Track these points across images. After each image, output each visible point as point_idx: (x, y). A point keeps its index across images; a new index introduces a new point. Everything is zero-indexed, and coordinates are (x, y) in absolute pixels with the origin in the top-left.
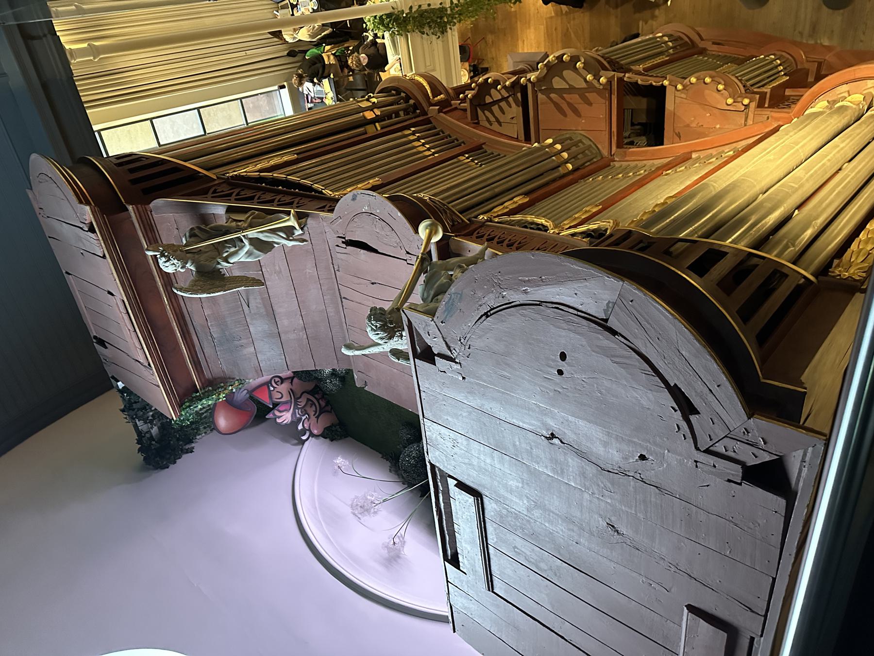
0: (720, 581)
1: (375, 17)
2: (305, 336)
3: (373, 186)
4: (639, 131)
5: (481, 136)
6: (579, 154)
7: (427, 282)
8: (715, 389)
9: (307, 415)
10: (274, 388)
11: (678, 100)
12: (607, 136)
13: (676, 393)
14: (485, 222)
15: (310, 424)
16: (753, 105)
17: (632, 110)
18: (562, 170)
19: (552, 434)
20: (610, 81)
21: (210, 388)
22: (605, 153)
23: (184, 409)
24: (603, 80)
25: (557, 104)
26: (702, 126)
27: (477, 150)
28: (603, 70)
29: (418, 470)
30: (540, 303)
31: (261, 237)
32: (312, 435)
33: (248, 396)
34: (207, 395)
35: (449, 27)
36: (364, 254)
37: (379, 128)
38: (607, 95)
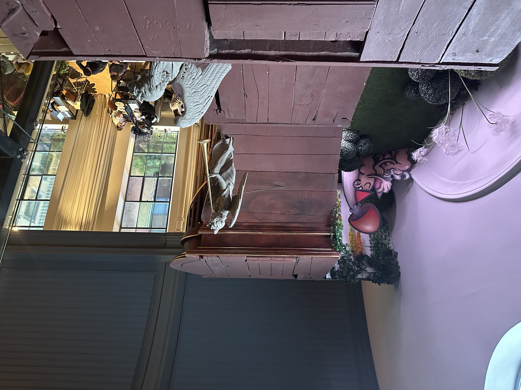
9: (391, 170)
15: (399, 170)
29: (439, 88)
32: (409, 171)
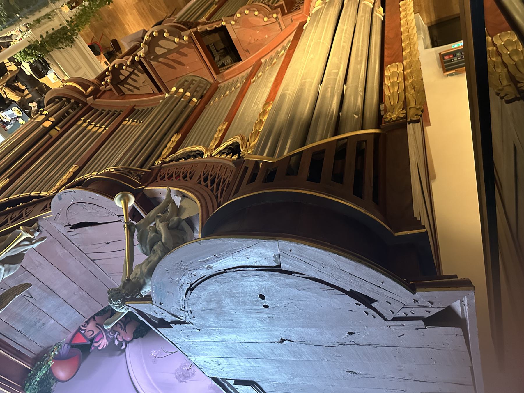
0: (436, 377)
1: (20, 52)
3: (74, 173)
4: (224, 54)
5: (130, 102)
6: (197, 88)
7: (141, 240)
9: (117, 333)
10: (85, 330)
11: (236, 31)
12: (207, 70)
13: (352, 294)
14: (161, 165)
15: (122, 337)
16: (280, 16)
17: (213, 43)
18: (191, 105)
19: (282, 339)
20: (190, 37)
21: (38, 363)
22: (211, 80)
24: (185, 38)
25: (166, 63)
26: (258, 40)
28: (182, 31)
30: (225, 271)
31: (10, 254)
32: (127, 342)
33: (69, 347)
34: (39, 369)
35: (74, 37)
36: (90, 229)
37: (59, 129)
38: (193, 46)
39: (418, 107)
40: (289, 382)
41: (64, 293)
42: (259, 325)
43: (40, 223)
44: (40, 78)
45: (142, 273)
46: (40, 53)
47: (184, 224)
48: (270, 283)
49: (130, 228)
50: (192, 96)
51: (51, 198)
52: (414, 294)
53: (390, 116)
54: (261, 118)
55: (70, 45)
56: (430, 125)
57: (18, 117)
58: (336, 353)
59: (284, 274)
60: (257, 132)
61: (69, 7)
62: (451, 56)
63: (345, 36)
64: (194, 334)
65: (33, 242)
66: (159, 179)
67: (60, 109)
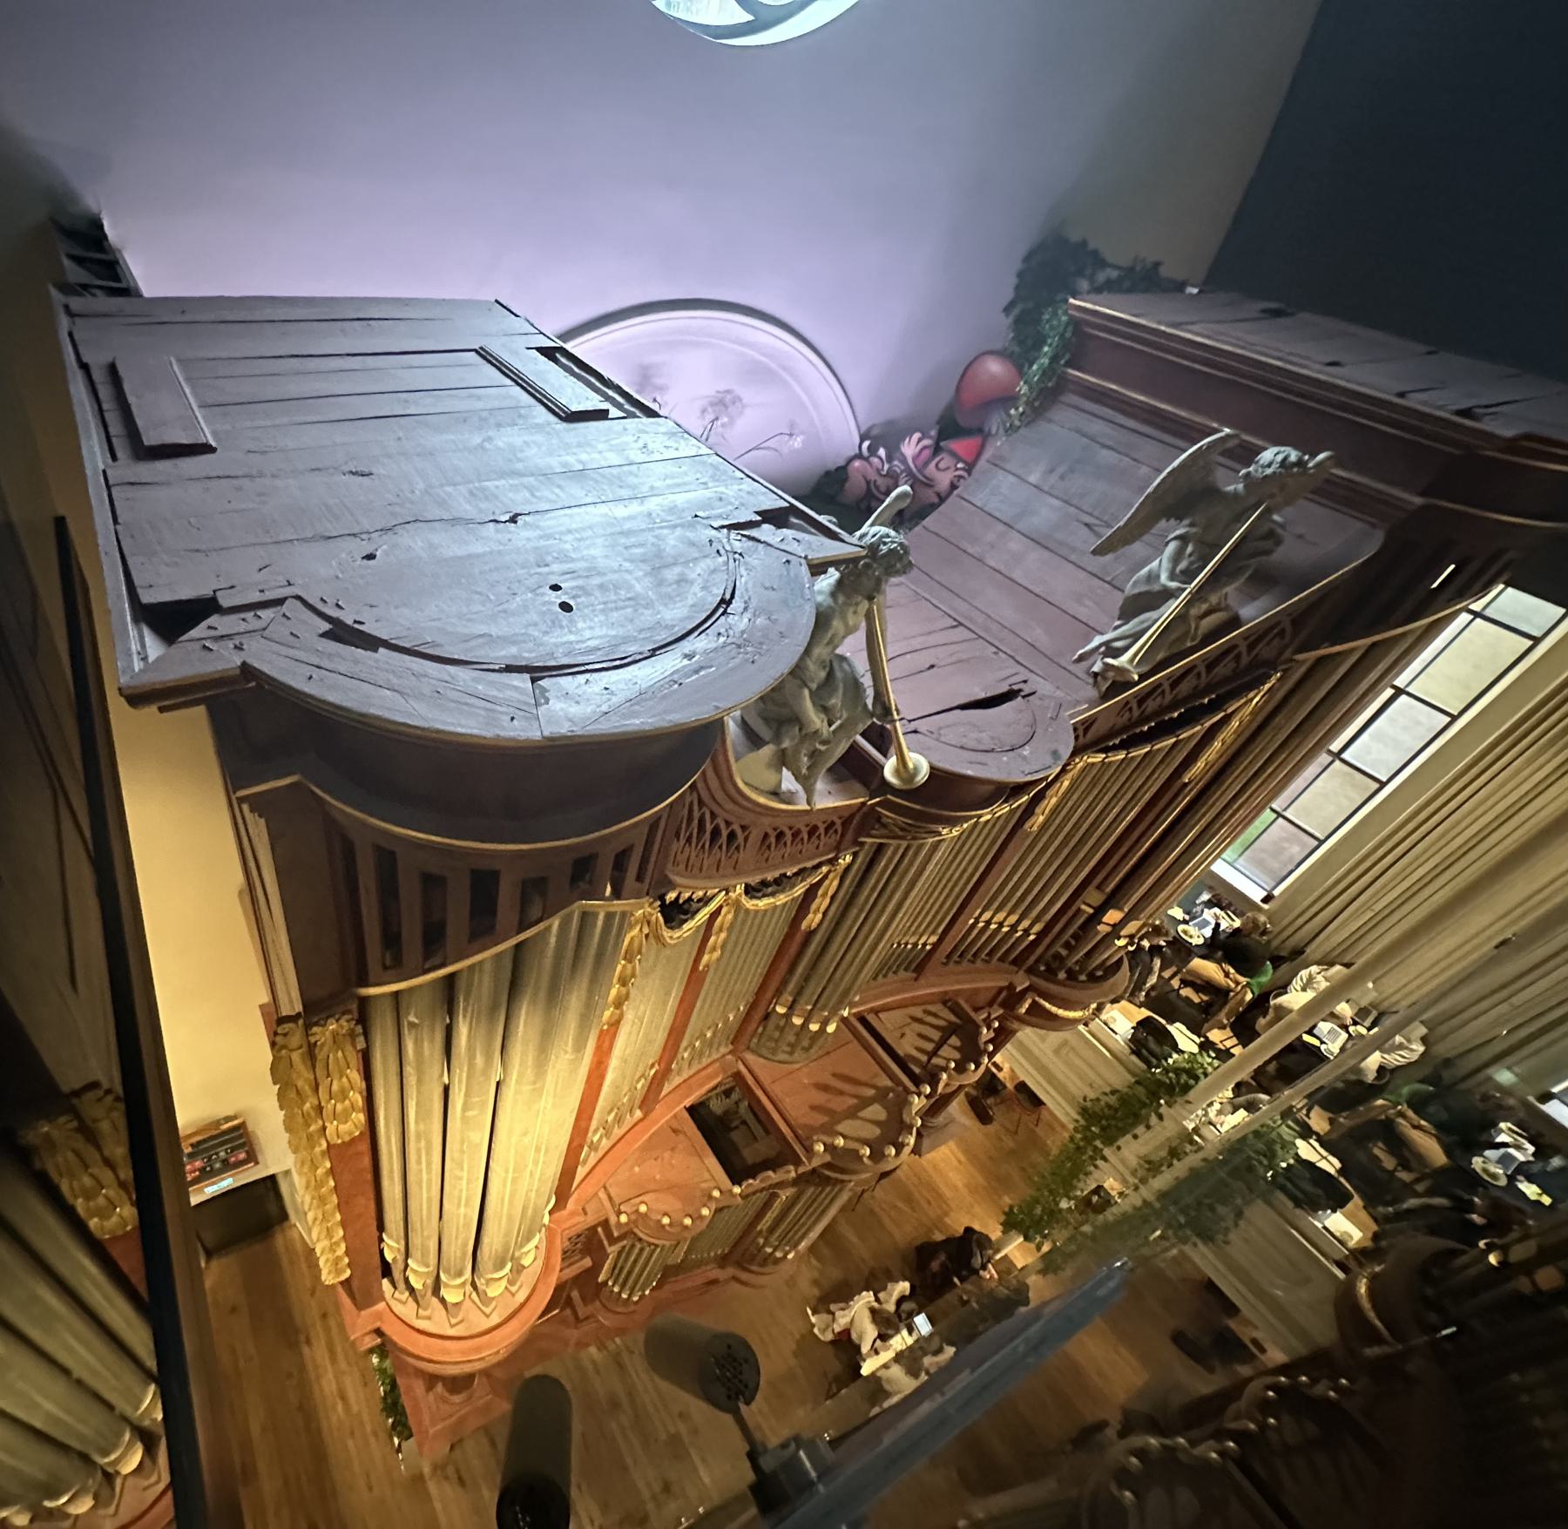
1: (1206, 1075)
2: (970, 550)
7: (855, 686)
8: (316, 673)
10: (957, 469)
11: (707, 1175)
13: (372, 643)
16: (613, 1219)
17: (755, 1138)
18: (787, 998)
19: (515, 522)
20: (809, 1151)
21: (1050, 384)
22: (749, 1057)
23: (1068, 324)
24: (820, 1148)
27: (919, 964)
30: (653, 653)
32: (859, 456)
33: (986, 429)
34: (1046, 373)
35: (1082, 1122)
37: (1083, 907)
39: (284, 1052)
40: (491, 433)
41: (1016, 544)
42: (568, 546)
43: (1093, 693)
44: (1148, 1019)
45: (844, 618)
46: (1158, 1077)
47: (764, 731)
48: (551, 639)
49: (885, 710)
50: (788, 1016)
51: (1076, 752)
52: (244, 664)
53: (342, 1027)
54: (624, 990)
55: (1089, 1104)
56: (261, 1007)
57: (1185, 922)
58: (397, 509)
59: (523, 663)
60: (629, 958)
61: (1105, 1190)
62: (233, 1159)
63: (461, 1191)
64: (707, 505)
65: (1103, 649)
66: (838, 822)
67: (1089, 954)
